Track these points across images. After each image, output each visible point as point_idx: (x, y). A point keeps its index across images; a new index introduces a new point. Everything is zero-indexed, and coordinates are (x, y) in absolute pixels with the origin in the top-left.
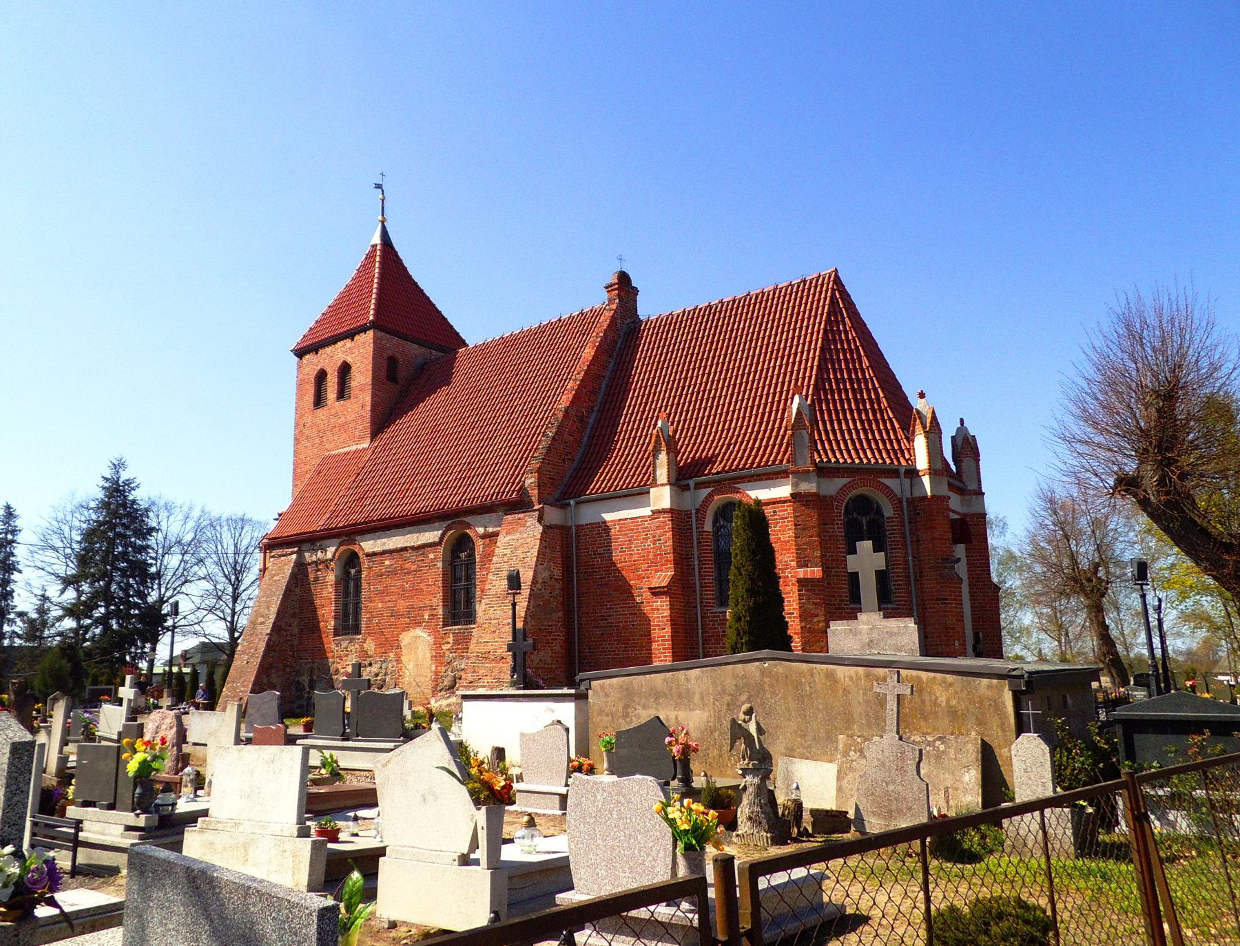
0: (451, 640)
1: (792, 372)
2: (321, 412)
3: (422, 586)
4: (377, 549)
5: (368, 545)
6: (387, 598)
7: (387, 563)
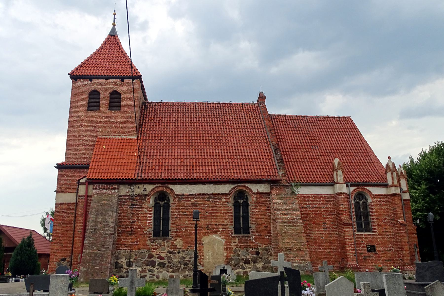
0: (237, 240)
2: (93, 114)
3: (218, 214)
4: (195, 192)
5: (178, 189)
7: (192, 200)
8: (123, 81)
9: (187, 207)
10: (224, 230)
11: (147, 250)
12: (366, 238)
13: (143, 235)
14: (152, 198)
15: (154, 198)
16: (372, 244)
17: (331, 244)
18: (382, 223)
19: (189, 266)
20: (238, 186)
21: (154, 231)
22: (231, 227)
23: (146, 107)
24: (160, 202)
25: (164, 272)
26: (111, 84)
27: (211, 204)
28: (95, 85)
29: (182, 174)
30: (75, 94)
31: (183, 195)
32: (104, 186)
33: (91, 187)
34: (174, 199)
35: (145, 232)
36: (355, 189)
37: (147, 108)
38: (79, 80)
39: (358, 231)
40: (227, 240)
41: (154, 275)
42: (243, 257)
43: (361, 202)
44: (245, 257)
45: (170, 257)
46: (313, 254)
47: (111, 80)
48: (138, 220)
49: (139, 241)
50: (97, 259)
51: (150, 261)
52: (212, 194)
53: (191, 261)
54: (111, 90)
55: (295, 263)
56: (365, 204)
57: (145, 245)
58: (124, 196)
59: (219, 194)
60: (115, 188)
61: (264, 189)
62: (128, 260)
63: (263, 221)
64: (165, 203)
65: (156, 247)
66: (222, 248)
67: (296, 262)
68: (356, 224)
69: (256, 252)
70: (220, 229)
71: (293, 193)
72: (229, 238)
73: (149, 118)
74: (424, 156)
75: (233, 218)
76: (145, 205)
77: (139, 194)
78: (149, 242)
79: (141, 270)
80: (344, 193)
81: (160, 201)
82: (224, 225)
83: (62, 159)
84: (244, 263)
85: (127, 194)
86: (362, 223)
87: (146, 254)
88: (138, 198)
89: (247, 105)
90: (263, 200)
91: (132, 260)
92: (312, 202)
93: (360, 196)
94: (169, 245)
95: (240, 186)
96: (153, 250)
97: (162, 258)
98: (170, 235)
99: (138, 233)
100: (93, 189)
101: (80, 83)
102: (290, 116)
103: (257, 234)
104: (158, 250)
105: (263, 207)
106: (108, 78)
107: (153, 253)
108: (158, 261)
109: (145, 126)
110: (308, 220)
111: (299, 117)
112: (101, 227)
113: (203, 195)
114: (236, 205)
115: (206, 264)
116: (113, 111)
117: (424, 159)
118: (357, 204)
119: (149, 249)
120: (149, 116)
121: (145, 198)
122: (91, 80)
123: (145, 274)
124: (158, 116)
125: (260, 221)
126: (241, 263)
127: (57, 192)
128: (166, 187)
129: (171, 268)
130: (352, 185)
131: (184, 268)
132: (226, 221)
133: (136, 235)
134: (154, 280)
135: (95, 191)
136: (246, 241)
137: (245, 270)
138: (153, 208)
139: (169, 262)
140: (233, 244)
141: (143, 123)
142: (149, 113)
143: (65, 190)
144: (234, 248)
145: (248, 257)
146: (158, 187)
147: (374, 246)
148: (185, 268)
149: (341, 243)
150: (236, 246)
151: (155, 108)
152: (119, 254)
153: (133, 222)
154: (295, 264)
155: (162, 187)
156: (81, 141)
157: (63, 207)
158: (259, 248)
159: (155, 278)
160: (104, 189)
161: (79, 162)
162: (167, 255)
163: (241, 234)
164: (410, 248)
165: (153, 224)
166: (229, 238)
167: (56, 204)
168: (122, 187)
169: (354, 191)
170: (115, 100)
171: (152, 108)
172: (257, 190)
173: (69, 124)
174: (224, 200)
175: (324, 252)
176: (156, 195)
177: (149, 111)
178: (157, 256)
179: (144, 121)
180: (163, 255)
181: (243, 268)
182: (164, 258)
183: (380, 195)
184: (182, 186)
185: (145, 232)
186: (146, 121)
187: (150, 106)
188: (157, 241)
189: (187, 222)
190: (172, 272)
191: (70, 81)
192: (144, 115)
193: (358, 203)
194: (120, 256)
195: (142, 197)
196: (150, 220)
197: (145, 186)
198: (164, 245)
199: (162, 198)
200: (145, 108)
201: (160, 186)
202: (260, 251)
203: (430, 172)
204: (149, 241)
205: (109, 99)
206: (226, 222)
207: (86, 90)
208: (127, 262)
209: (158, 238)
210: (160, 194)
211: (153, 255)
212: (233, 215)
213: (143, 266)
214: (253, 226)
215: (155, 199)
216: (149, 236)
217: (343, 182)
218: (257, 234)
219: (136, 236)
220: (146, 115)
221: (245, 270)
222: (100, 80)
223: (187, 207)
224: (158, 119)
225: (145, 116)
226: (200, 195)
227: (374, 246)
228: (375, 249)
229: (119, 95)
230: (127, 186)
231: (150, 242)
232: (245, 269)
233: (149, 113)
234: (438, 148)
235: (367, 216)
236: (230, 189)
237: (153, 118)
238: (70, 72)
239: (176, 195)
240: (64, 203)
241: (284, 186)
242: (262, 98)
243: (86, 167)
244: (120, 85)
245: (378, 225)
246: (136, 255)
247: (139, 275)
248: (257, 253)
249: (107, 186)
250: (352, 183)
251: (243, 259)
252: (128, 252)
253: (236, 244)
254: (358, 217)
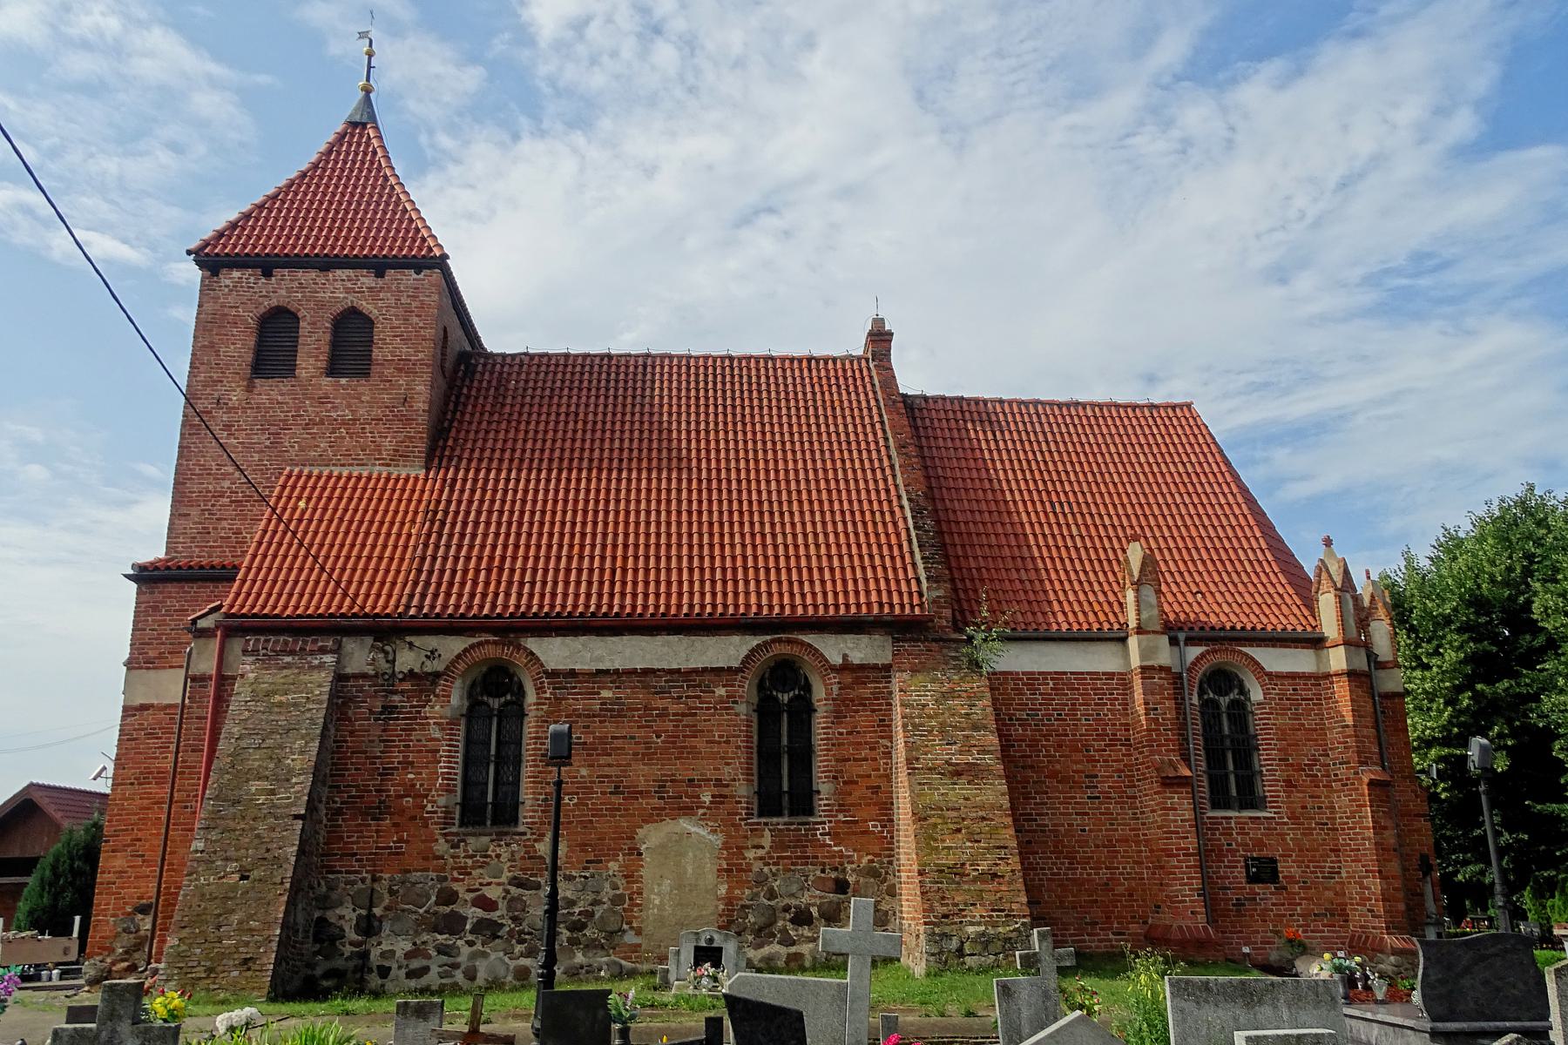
0: (767, 840)
1: (259, 569)
2: (271, 391)
3: (700, 743)
4: (618, 664)
5: (555, 652)
6: (603, 760)
7: (606, 694)
8: (380, 274)
9: (588, 716)
10: (719, 799)
11: (433, 875)
12: (1242, 833)
13: (422, 818)
14: (458, 683)
15: (468, 682)
16: (1265, 853)
17: (1114, 854)
18: (1302, 778)
19: (587, 932)
20: (773, 641)
21: (464, 805)
22: (743, 790)
23: (471, 371)
24: (491, 701)
25: (493, 957)
26: (338, 285)
27: (674, 708)
28: (283, 289)
29: (571, 600)
30: (209, 326)
31: (572, 673)
32: (286, 643)
33: (237, 645)
34: (540, 689)
35: (429, 808)
36: (1203, 655)
37: (474, 372)
38: (224, 271)
39: (1215, 806)
40: (729, 836)
41: (455, 966)
42: (787, 901)
43: (1224, 701)
44: (793, 902)
45: (519, 898)
46: (248, 447)
47: (339, 272)
48: (407, 764)
49: (407, 842)
50: (233, 911)
51: (445, 916)
52: (678, 671)
53: (597, 916)
54: (339, 308)
55: (972, 924)
56: (1240, 711)
57: (429, 856)
58: (356, 676)
59: (705, 670)
60: (323, 651)
61: (869, 650)
62: (364, 912)
63: (865, 768)
64: (507, 703)
65: (470, 862)
66: (710, 868)
67: (978, 919)
68: (1205, 778)
69: (837, 881)
70: (706, 798)
71: (975, 665)
72: (737, 831)
73: (474, 406)
74: (1452, 546)
75: (755, 756)
76: (436, 710)
77: (411, 671)
78: (441, 847)
79: (408, 947)
80: (1161, 668)
81: (490, 695)
82: (719, 783)
83: (155, 551)
84: (792, 921)
85: (370, 670)
86: (1227, 776)
87: (432, 887)
88: (407, 686)
89: (826, 363)
90: (866, 692)
91: (377, 911)
92: (1048, 700)
93: (1222, 680)
94: (517, 857)
95: (780, 641)
96: (455, 874)
97: (489, 905)
98: (522, 820)
99: (402, 811)
100: (245, 652)
101: (228, 282)
102: (977, 401)
103: (841, 817)
104: (475, 873)
105: (863, 719)
106: (326, 264)
107: (456, 886)
108: (473, 913)
109: (458, 432)
110: (1032, 767)
111: (1010, 402)
112: (260, 792)
113: (647, 672)
114: (766, 711)
115: (649, 928)
116: (343, 381)
117: (1455, 559)
118: (1209, 707)
119: (443, 869)
120: (477, 398)
121: (434, 683)
122: (268, 274)
123: (425, 963)
124: (509, 401)
125: (853, 770)
126: (780, 923)
127: (131, 665)
128: (511, 643)
129: (521, 942)
130: (1191, 641)
131: (569, 940)
132: (727, 769)
133: (397, 819)
134: (456, 984)
135: (251, 659)
136: (799, 843)
137: (793, 949)
138: (463, 721)
139: (514, 919)
140: (750, 854)
141: (451, 421)
142: (479, 390)
143: (161, 656)
144: (755, 869)
145: (805, 899)
146: (480, 644)
147: (1273, 861)
148: (573, 942)
149: (1151, 851)
150: (761, 858)
151: (501, 373)
152: (331, 889)
153: (386, 773)
154: (971, 929)
155: (495, 643)
156: (226, 484)
157: (149, 718)
158: (849, 867)
159: (459, 976)
160: (285, 652)
161: (216, 561)
162: (508, 892)
163: (780, 814)
164: (1405, 869)
165: (459, 778)
166: (737, 831)
167: (125, 709)
168: (350, 644)
169: (1198, 659)
170: (351, 343)
171: (492, 373)
172: (845, 656)
173: (183, 425)
174: (721, 691)
175: (1089, 881)
176: (476, 673)
177: (481, 382)
178: (473, 895)
179: (458, 415)
180: (493, 893)
181: (788, 941)
182: (495, 903)
183: (1293, 676)
184: (568, 640)
185: (429, 808)
186: (463, 414)
187: (485, 365)
188: (471, 840)
189: (584, 772)
190: (521, 955)
191: (192, 274)
192: (458, 397)
193: (1216, 705)
194: (334, 896)
195: (425, 682)
196: (449, 764)
197: (432, 642)
198: (498, 856)
199: (495, 687)
200: (465, 373)
201: (487, 642)
202: (851, 879)
203: (1477, 603)
204: (442, 841)
205: (328, 337)
206: (727, 772)
207: (251, 306)
208: (359, 917)
209: (478, 829)
210: (491, 670)
211: (456, 893)
212: (755, 745)
213: (417, 933)
214: (824, 787)
215: (473, 685)
216: (447, 820)
217: (1158, 628)
218: (841, 817)
219: (395, 825)
220: (468, 397)
221: (793, 949)
222: (300, 273)
223: (588, 716)
224: (507, 409)
225: (462, 399)
226: (633, 672)
227: (1273, 861)
228: (1275, 872)
229: (368, 323)
230: (369, 640)
231: (446, 846)
232: (793, 943)
233: (479, 390)
234: (1502, 517)
235: (1245, 749)
236: (744, 652)
237: (488, 408)
238: (194, 244)
239: (546, 672)
240: (152, 706)
241: (941, 640)
242: (880, 338)
243: (223, 575)
244: (370, 289)
245: (1289, 783)
246: (392, 892)
247: (400, 967)
248: (841, 887)
249: (295, 642)
250: (1193, 634)
251: (787, 909)
252: (363, 880)
253: (761, 852)
254: (1214, 758)
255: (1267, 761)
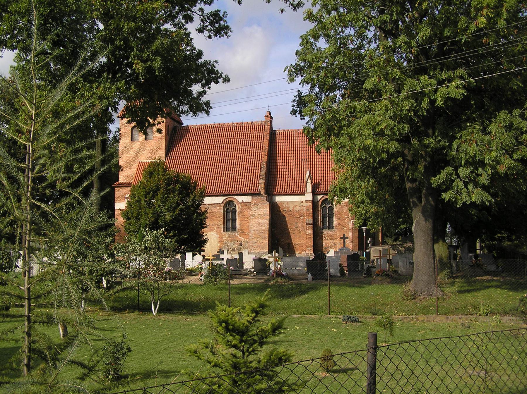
43: (327, 207)
90: (246, 207)
255: (335, 218)
